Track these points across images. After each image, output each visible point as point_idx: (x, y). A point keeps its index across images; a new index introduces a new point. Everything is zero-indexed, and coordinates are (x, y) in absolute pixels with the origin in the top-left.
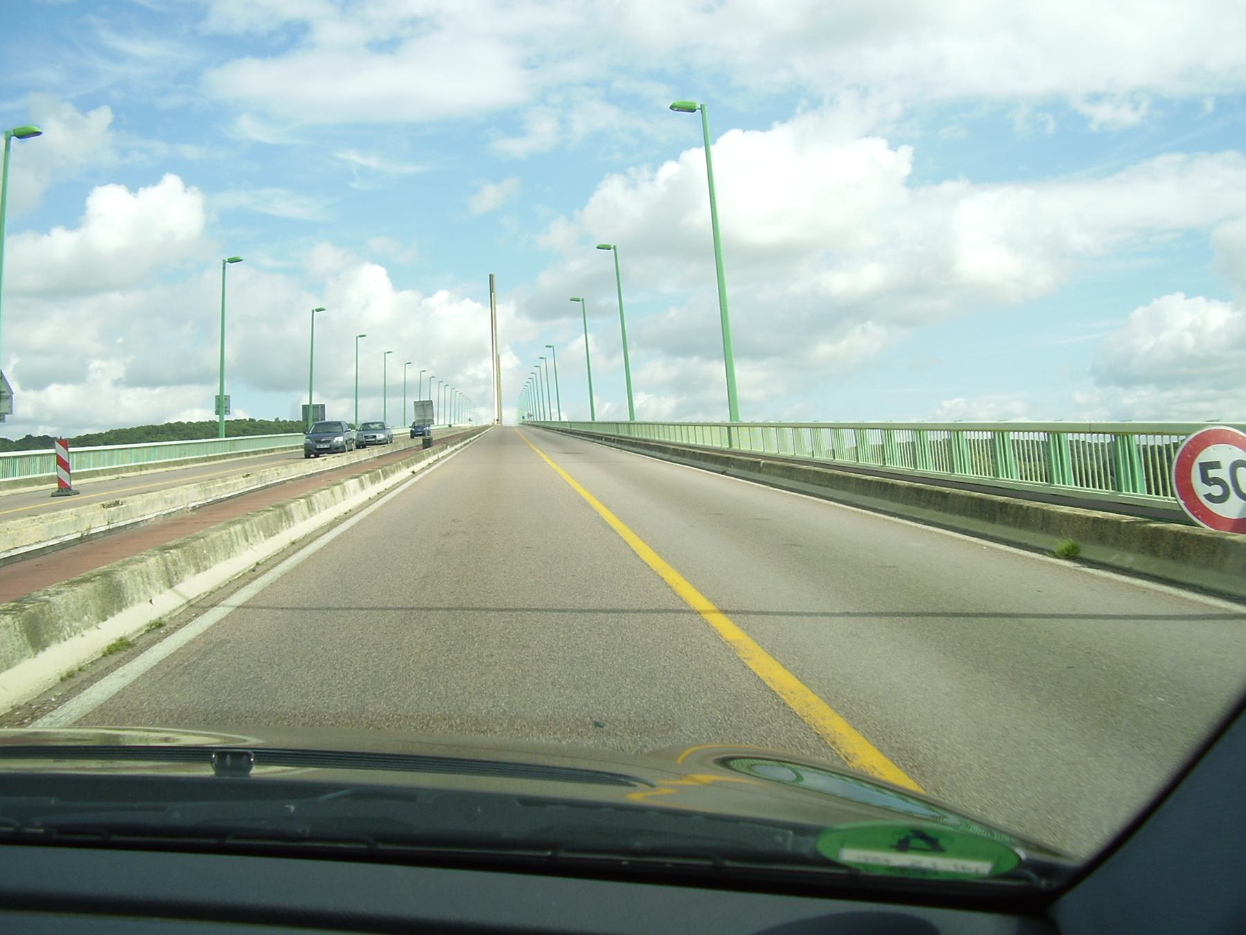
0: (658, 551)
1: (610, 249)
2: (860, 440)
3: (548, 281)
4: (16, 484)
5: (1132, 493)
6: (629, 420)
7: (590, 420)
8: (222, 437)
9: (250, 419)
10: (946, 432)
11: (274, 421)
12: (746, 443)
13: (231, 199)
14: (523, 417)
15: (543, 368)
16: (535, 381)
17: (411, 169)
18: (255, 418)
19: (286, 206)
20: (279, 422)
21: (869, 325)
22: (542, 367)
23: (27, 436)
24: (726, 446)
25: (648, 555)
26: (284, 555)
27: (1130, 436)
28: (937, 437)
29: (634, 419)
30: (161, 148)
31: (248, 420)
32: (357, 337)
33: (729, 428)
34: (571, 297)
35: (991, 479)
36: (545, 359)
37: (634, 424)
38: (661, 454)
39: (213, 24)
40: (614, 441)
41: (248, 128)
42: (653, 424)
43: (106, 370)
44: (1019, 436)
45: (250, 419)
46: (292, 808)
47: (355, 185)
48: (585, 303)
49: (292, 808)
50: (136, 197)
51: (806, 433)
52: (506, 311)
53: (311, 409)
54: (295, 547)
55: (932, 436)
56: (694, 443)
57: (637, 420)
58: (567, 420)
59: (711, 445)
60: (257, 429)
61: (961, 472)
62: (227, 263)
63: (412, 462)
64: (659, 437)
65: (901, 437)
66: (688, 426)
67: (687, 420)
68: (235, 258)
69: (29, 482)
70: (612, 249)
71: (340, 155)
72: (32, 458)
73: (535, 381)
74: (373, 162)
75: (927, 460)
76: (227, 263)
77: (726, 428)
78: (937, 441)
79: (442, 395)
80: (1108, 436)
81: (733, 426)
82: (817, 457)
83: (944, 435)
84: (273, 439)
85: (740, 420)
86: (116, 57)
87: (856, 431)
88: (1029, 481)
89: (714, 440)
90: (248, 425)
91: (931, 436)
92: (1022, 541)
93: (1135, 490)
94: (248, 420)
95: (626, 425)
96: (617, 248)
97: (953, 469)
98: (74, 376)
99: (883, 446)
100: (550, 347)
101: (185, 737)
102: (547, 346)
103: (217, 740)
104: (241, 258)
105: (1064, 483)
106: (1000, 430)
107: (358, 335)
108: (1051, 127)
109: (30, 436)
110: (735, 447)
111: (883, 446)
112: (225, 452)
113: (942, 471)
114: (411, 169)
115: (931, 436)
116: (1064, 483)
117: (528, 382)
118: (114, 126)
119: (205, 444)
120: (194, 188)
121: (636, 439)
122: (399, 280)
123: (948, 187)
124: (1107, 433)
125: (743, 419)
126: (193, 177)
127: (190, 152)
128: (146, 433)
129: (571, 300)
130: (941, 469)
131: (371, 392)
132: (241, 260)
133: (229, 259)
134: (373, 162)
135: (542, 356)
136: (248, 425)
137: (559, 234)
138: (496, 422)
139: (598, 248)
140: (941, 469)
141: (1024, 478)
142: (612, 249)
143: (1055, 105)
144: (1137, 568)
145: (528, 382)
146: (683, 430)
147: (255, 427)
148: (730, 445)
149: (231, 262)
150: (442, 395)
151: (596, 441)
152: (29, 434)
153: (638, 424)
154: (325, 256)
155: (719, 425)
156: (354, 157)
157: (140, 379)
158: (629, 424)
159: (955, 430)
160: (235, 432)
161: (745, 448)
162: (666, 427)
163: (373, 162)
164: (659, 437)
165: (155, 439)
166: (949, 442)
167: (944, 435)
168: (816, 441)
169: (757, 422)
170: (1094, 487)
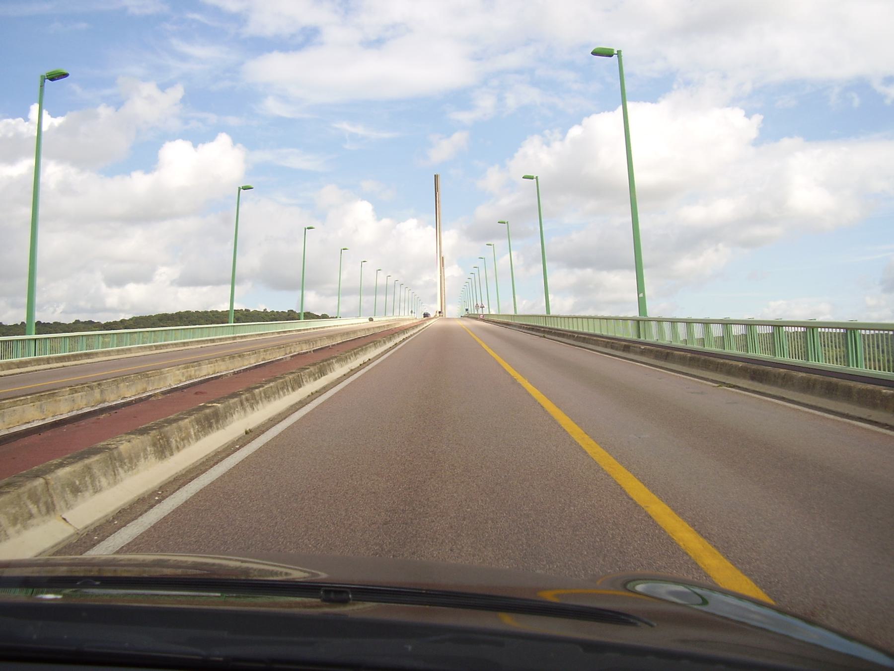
0: (679, 511)
1: (611, 56)
2: (707, 332)
3: (485, 213)
4: (150, 348)
5: (825, 364)
6: (638, 316)
7: (488, 313)
8: (231, 323)
9: (245, 310)
11: (263, 311)
12: (653, 336)
13: (262, 156)
14: (467, 310)
17: (386, 135)
18: (249, 309)
19: (297, 160)
20: (267, 312)
21: (721, 246)
23: (76, 320)
25: (473, 335)
26: (301, 405)
27: (855, 331)
29: (549, 314)
30: (213, 118)
31: (244, 310)
32: (305, 229)
36: (478, 268)
39: (251, 29)
40: (596, 343)
41: (273, 107)
43: (165, 273)
44: (786, 329)
45: (245, 310)
46: (410, 648)
48: (539, 181)
49: (410, 648)
50: (196, 151)
52: (450, 238)
54: (352, 372)
56: (582, 330)
57: (552, 313)
58: (494, 313)
60: (248, 317)
62: (241, 190)
64: (561, 326)
65: (737, 330)
67: (582, 314)
69: (39, 362)
73: (468, 287)
74: (360, 130)
75: (756, 346)
76: (241, 190)
79: (407, 294)
80: (802, 328)
83: (769, 330)
84: (267, 325)
85: (648, 315)
87: (775, 328)
90: (242, 314)
91: (760, 330)
92: (794, 399)
94: (244, 310)
96: (538, 178)
98: (144, 278)
99: (723, 337)
100: (482, 258)
102: (480, 258)
105: (857, 367)
106: (811, 327)
108: (856, 102)
109: (78, 321)
111: (723, 337)
112: (282, 329)
113: (797, 359)
114: (386, 135)
115: (760, 330)
116: (857, 367)
117: (463, 288)
118: (183, 100)
120: (240, 145)
121: (550, 329)
122: (380, 211)
123: (786, 142)
124: (842, 328)
126: (237, 138)
127: (233, 121)
128: (159, 319)
129: (499, 222)
130: (780, 355)
131: (349, 292)
132: (252, 188)
133: (242, 187)
136: (242, 314)
137: (493, 178)
138: (438, 315)
139: (523, 178)
142: (506, 224)
143: (861, 85)
145: (463, 288)
147: (247, 316)
148: (583, 329)
149: (244, 189)
150: (407, 294)
151: (546, 335)
152: (77, 319)
154: (329, 194)
156: (346, 127)
157: (189, 281)
158: (514, 316)
159: (777, 326)
162: (591, 321)
163: (360, 130)
164: (561, 326)
165: (165, 324)
166: (773, 334)
167: (769, 330)
168: (690, 332)
170: (799, 359)
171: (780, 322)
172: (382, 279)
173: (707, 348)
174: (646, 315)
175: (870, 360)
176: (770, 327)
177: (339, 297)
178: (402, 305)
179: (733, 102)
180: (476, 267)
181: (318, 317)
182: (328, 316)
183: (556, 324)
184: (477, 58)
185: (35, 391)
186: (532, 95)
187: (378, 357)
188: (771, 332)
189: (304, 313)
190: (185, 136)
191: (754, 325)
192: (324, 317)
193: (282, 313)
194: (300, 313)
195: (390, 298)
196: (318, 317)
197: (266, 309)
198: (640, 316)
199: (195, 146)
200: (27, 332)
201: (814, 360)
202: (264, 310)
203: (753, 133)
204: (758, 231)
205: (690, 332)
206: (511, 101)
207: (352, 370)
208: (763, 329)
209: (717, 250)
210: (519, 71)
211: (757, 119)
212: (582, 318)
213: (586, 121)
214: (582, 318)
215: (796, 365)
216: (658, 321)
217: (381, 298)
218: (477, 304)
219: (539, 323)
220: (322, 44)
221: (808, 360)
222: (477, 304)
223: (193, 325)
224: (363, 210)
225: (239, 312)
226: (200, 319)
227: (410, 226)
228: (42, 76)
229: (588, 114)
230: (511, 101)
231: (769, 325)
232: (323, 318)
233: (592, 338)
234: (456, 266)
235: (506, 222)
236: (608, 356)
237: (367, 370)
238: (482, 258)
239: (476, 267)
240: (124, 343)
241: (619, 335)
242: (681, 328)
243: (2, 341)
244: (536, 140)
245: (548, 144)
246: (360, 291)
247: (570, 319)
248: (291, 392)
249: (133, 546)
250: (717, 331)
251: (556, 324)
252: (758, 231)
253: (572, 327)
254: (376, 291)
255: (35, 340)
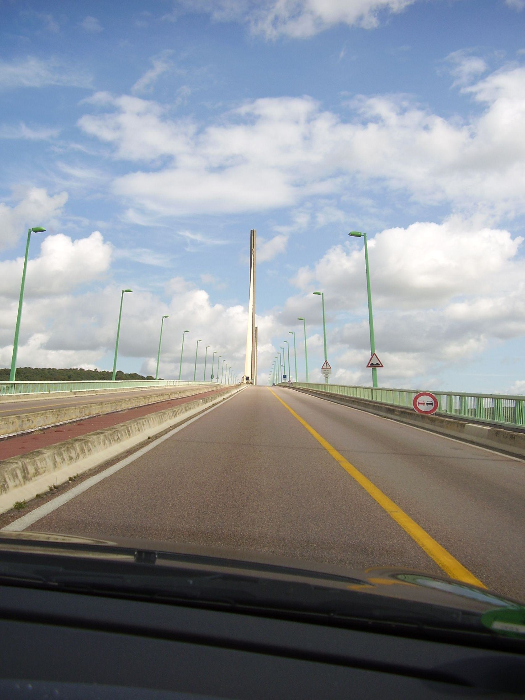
0: (428, 530)
8: (114, 380)
10: (513, 401)
11: (94, 370)
12: (379, 398)
13: (124, 253)
15: (286, 350)
16: (282, 356)
17: (219, 242)
21: (482, 336)
22: (281, 354)
24: (370, 399)
28: (510, 405)
33: (372, 390)
34: (289, 332)
35: (512, 424)
37: (327, 385)
38: (413, 421)
39: (123, 154)
42: (350, 387)
47: (188, 250)
51: (340, 387)
53: (512, 408)
54: (150, 440)
55: (511, 404)
59: (380, 401)
61: (520, 424)
62: (124, 292)
63: (218, 395)
66: (360, 388)
68: (128, 290)
70: (321, 295)
71: (181, 233)
72: (37, 385)
73: (282, 356)
75: (501, 415)
77: (371, 390)
78: (505, 407)
81: (358, 388)
82: (449, 413)
86: (66, 177)
88: (509, 422)
89: (365, 396)
93: (523, 424)
95: (323, 386)
97: (516, 421)
100: (282, 348)
101: (72, 539)
103: (92, 542)
104: (131, 290)
107: (185, 331)
110: (374, 399)
114: (219, 242)
119: (83, 384)
125: (380, 385)
127: (101, 224)
129: (290, 333)
130: (509, 421)
134: (198, 237)
135: (279, 352)
138: (245, 382)
139: (314, 293)
140: (509, 421)
141: (490, 418)
142: (321, 295)
144: (398, 419)
146: (351, 389)
153: (329, 385)
155: (368, 388)
156: (188, 234)
158: (325, 385)
160: (63, 377)
161: (379, 400)
166: (514, 408)
168: (463, 403)
169: (404, 389)
171: (521, 397)
172: (210, 351)
173: (462, 415)
174: (377, 386)
175: (506, 419)
176: (492, 399)
177: (181, 364)
178: (224, 372)
179: (500, 226)
180: (276, 357)
181: (143, 378)
182: (153, 378)
183: (349, 393)
184: (297, 185)
185: (50, 409)
186: (338, 216)
187: (201, 412)
188: (513, 406)
189: (17, 369)
190: (66, 233)
191: (500, 399)
192: (150, 378)
193: (29, 369)
194: (10, 370)
195: (215, 366)
196: (143, 378)
197: (97, 369)
198: (373, 386)
199: (73, 241)
200: (10, 379)
201: (519, 423)
202: (95, 370)
203: (513, 252)
204: (512, 326)
205: (463, 403)
206: (321, 219)
207: (149, 438)
208: (507, 402)
209: (478, 340)
210: (329, 197)
211: (519, 240)
212: (364, 388)
213: (377, 235)
214: (368, 389)
215: (486, 422)
216: (448, 395)
217: (209, 366)
218: (326, 363)
219: (333, 391)
220: (175, 168)
221: (516, 423)
222: (326, 363)
223: (50, 381)
224: (201, 296)
225: (72, 371)
226: (35, 375)
227: (237, 310)
228: (29, 229)
229: (381, 231)
230: (321, 219)
231: (512, 400)
232: (148, 380)
233: (397, 409)
234: (270, 345)
235: (303, 319)
236: (375, 416)
237: (204, 415)
238: (282, 348)
239: (276, 357)
240: (19, 390)
241: (397, 403)
242: (456, 401)
243: (1, 384)
244: (338, 249)
245: (348, 254)
246: (196, 360)
247: (351, 388)
248: (108, 446)
249: (32, 527)
250: (471, 403)
251: (349, 393)
252: (512, 326)
253: (367, 395)
254: (206, 360)
255: (15, 384)
